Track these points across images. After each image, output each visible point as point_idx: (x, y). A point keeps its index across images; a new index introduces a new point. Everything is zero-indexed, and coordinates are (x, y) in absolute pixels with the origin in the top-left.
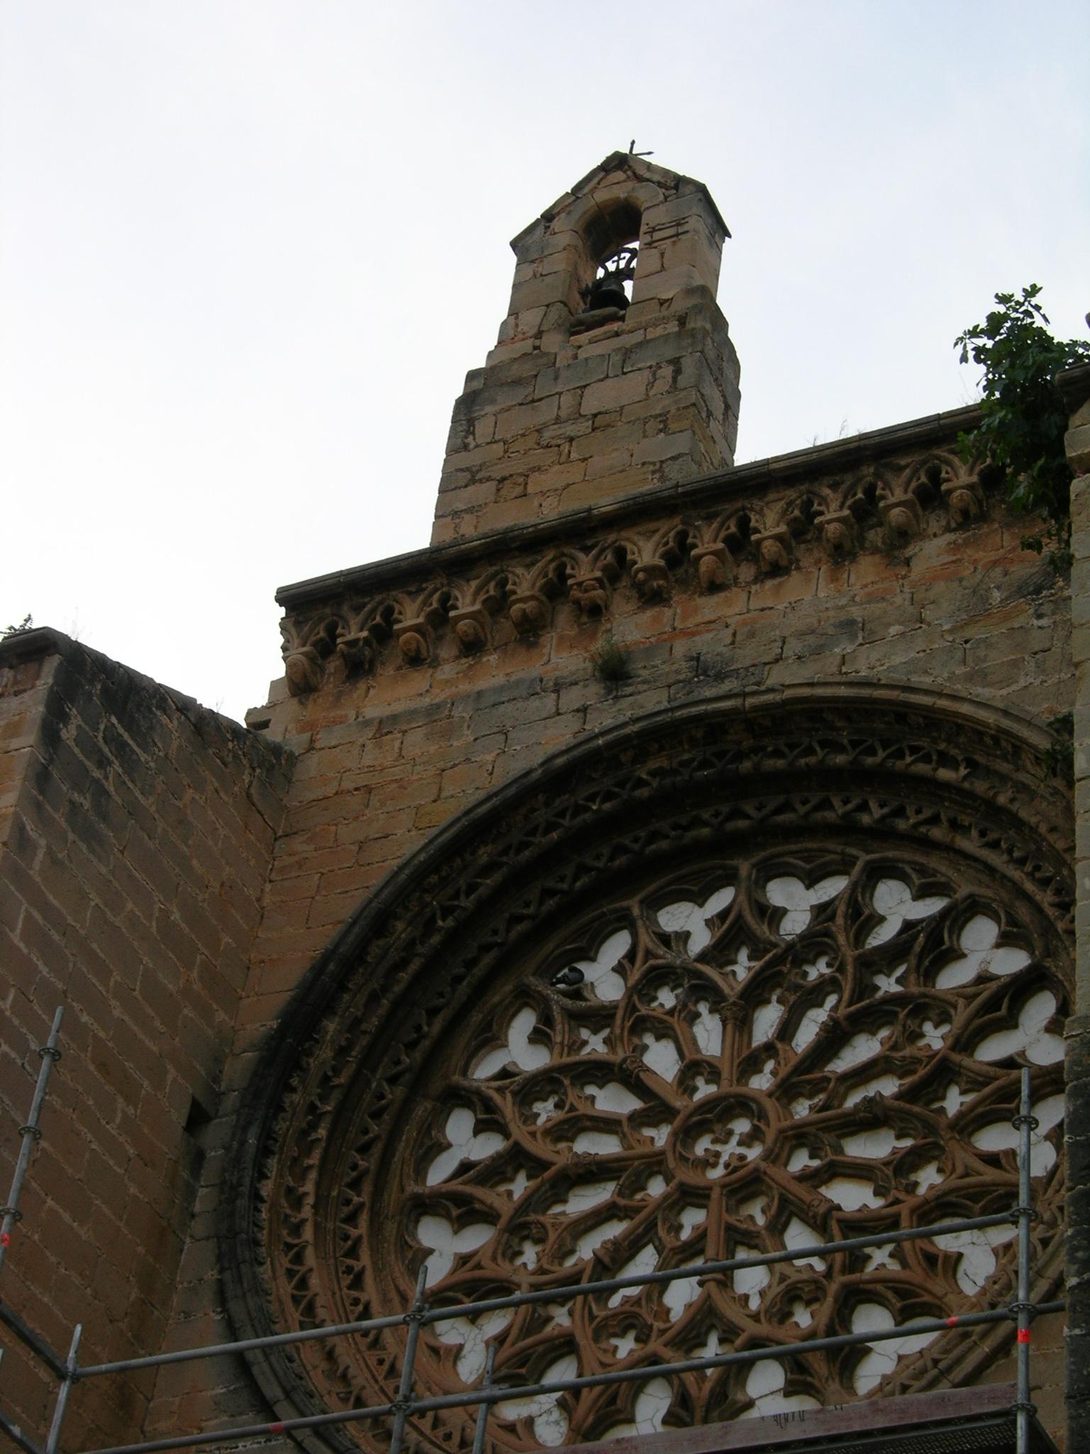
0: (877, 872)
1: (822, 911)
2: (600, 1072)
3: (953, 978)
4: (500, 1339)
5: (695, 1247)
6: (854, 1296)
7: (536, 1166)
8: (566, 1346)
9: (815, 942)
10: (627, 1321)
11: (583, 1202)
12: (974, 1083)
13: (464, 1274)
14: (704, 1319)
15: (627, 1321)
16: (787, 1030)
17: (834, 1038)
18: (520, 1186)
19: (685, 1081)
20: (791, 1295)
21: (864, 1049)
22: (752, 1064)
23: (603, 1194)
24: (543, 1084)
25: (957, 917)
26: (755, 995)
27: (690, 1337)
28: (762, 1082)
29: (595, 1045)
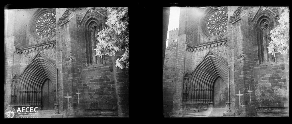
0: (52, 13)
1: (50, 14)
2: (42, 22)
5: (46, 29)
7: (211, 24)
8: (213, 31)
9: (49, 16)
10: (44, 33)
11: (213, 26)
14: (218, 30)
15: (44, 33)
16: (49, 20)
17: (51, 20)
18: (39, 27)
19: (216, 20)
23: (42, 27)
24: (211, 21)
25: (223, 11)
26: (47, 19)
27: (46, 33)
28: (219, 20)
29: (42, 21)
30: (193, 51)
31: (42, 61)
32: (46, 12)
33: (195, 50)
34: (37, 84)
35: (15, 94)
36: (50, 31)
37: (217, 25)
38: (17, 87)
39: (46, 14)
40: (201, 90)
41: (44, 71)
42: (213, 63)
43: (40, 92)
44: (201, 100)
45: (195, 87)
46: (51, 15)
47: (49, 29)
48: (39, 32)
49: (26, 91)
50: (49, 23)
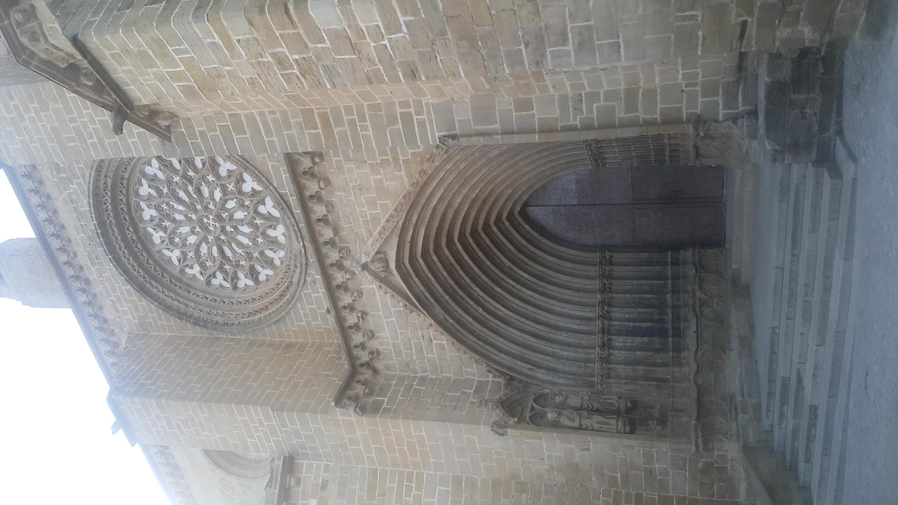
3: (161, 176)
4: (263, 267)
6: (240, 192)
7: (222, 264)
8: (262, 253)
9: (158, 208)
11: (228, 253)
12: (185, 170)
13: (249, 276)
17: (180, 201)
19: (197, 234)
20: (242, 206)
21: (182, 194)
22: (190, 220)
24: (203, 266)
28: (194, 217)
30: (375, 371)
31: (408, 246)
32: (128, 204)
33: (364, 357)
34: (548, 348)
35: (617, 413)
36: (243, 205)
37: (223, 229)
38: (574, 401)
39: (143, 205)
40: (610, 319)
41: (471, 234)
42: (447, 245)
43: (607, 254)
44: (675, 277)
45: (591, 361)
46: (150, 197)
47: (234, 210)
48: (235, 273)
49: (603, 331)
50: (196, 211)
